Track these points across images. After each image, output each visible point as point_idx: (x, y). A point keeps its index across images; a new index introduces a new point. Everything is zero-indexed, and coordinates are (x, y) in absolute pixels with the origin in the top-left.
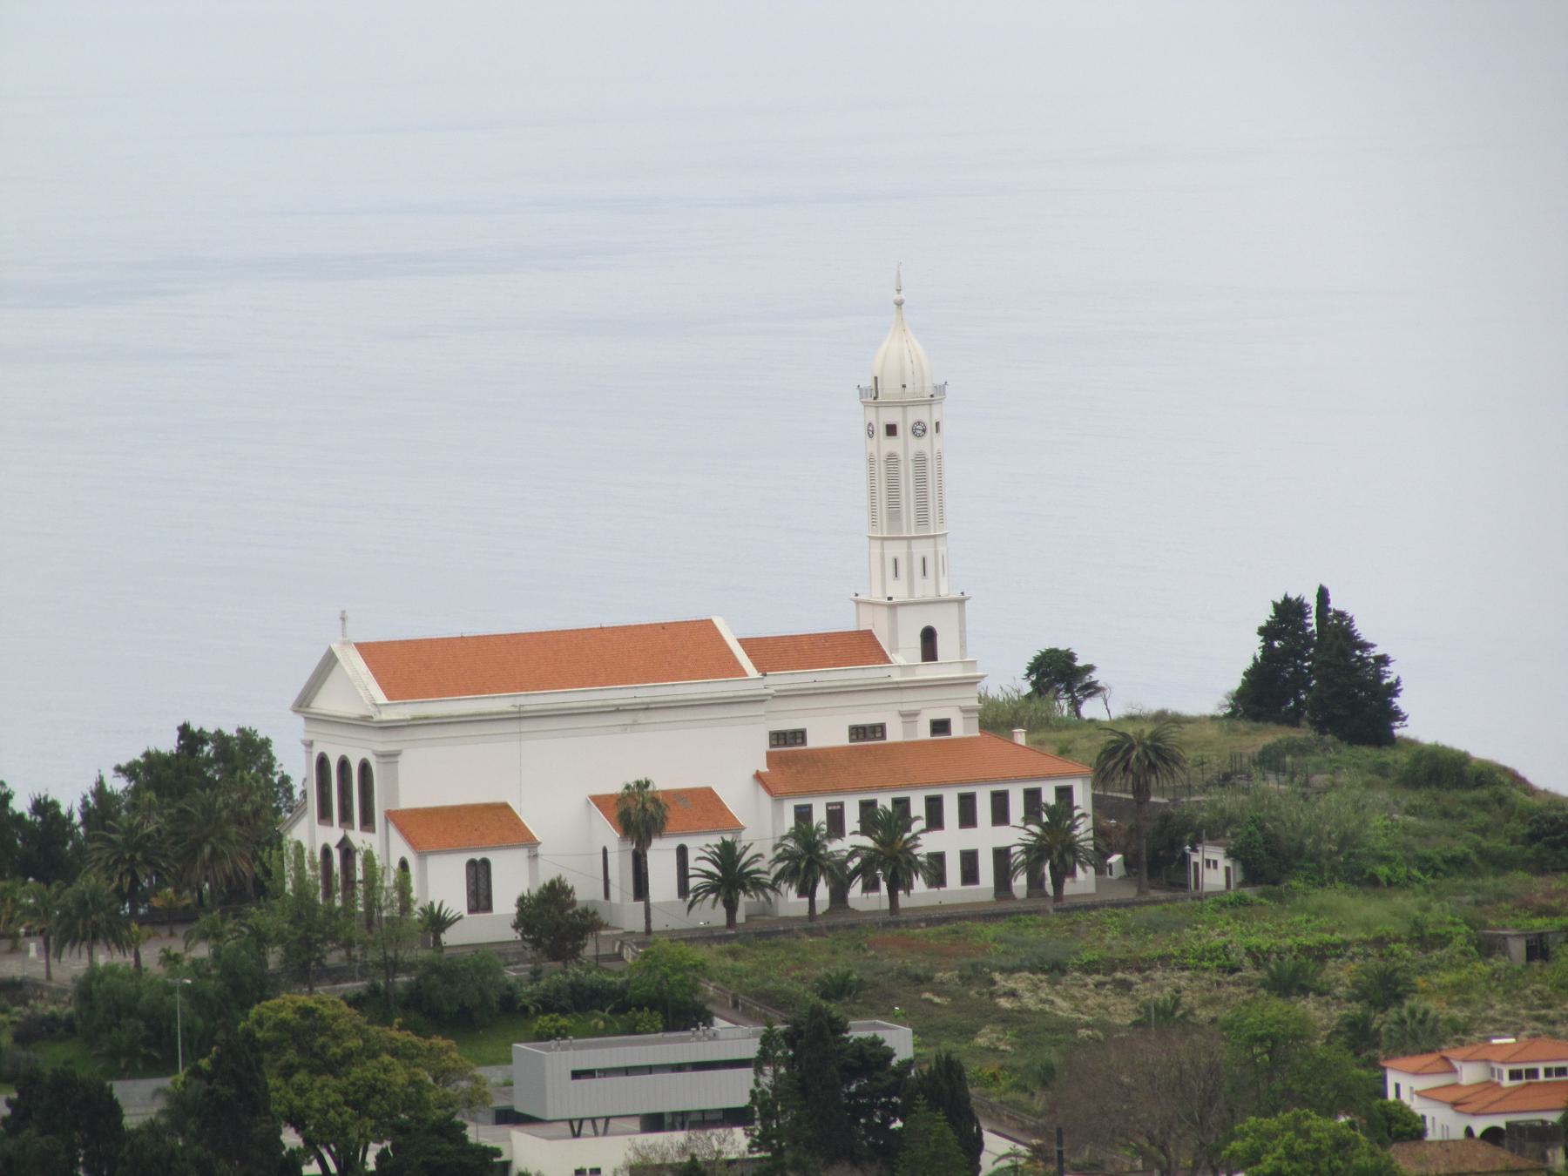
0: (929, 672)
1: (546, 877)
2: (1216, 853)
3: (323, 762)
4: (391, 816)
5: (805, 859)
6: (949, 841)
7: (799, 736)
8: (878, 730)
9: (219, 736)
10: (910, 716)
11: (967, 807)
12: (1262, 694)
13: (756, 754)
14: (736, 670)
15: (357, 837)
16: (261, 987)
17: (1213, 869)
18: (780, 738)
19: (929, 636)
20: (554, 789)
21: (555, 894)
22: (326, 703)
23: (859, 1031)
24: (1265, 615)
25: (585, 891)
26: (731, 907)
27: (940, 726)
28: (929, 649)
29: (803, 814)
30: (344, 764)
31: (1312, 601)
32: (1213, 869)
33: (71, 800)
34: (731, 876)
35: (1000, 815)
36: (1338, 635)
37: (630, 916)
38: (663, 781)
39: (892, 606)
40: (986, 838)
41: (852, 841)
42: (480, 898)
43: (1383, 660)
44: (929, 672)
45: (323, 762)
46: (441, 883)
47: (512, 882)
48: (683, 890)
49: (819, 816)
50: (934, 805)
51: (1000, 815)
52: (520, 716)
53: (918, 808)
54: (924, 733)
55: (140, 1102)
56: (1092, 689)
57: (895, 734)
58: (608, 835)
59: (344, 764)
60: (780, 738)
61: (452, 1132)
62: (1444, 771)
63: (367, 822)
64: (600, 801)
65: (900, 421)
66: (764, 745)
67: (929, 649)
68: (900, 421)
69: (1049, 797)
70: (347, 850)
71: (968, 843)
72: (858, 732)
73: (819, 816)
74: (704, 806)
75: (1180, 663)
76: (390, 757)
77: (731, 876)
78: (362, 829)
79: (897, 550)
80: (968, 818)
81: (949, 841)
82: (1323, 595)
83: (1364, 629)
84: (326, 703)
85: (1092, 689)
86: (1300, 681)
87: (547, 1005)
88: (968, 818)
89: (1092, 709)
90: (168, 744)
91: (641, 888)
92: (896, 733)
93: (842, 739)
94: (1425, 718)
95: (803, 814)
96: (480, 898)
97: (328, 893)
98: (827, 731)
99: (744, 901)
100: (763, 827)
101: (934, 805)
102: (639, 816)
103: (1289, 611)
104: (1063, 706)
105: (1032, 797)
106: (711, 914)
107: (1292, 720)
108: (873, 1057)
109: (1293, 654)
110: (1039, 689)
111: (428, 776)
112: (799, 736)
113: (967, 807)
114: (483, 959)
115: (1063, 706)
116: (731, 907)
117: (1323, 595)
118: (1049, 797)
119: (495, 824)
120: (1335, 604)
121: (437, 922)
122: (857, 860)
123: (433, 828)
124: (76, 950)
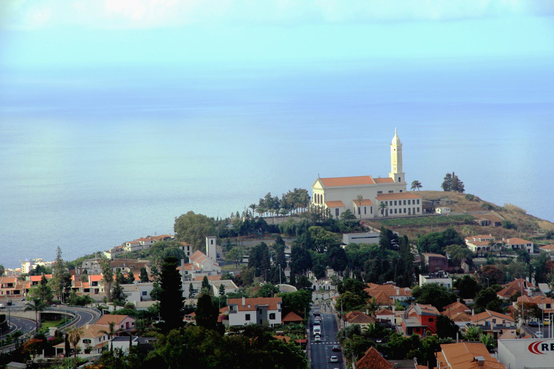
3: (315, 195)
8: (392, 191)
12: (445, 186)
13: (376, 194)
21: (348, 211)
24: (445, 176)
30: (318, 195)
31: (452, 174)
33: (280, 198)
42: (337, 214)
43: (462, 183)
44: (400, 183)
49: (384, 202)
50: (391, 202)
52: (333, 189)
56: (421, 186)
59: (318, 195)
62: (471, 198)
66: (376, 193)
72: (390, 192)
75: (433, 184)
82: (454, 173)
83: (459, 178)
91: (359, 213)
93: (388, 193)
97: (359, 213)
101: (391, 202)
103: (449, 175)
117: (454, 173)
120: (455, 175)
124: (219, 219)
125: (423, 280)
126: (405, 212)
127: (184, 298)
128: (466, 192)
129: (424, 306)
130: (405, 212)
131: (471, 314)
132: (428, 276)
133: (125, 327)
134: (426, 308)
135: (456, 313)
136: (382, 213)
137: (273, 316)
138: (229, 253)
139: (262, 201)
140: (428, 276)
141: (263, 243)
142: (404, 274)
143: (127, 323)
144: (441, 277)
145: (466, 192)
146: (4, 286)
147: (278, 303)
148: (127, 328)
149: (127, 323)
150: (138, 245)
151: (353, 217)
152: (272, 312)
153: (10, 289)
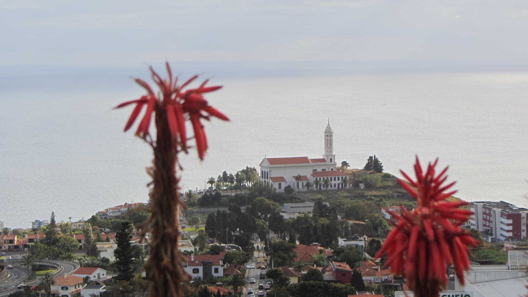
0: (331, 163)
1: (287, 185)
2: (362, 184)
3: (262, 172)
4: (270, 178)
5: (317, 182)
6: (333, 182)
7: (316, 170)
8: (325, 170)
9: (251, 168)
10: (329, 168)
11: (335, 178)
12: (367, 167)
13: (311, 172)
14: (309, 162)
15: (266, 180)
16: (256, 196)
17: (362, 186)
18: (314, 170)
19: (331, 159)
20: (289, 175)
21: (289, 187)
22: (263, 165)
23: (324, 203)
24: (368, 158)
25: (292, 187)
26: (308, 188)
27: (332, 169)
28: (331, 161)
29: (316, 179)
32: (362, 186)
34: (308, 185)
35: (339, 180)
36: (376, 161)
37: (296, 190)
38: (302, 175)
39: (327, 156)
40: (337, 182)
41: (322, 183)
42: (280, 187)
44: (331, 163)
45: (262, 172)
46: (276, 185)
47: (284, 185)
48: (303, 187)
49: (318, 179)
50: (331, 178)
51: (339, 180)
52: (285, 167)
53: (329, 178)
54: (330, 170)
55: (243, 209)
56: (349, 166)
57: (327, 170)
58: (294, 181)
60: (314, 170)
61: (278, 213)
63: (267, 178)
64: (294, 177)
65: (329, 135)
67: (331, 161)
68: (329, 135)
69: (344, 177)
70: (265, 181)
71: (335, 183)
72: (323, 170)
73: (318, 179)
74: (305, 178)
75: (358, 164)
76: (270, 171)
77: (308, 185)
78: (137, 134)
79: (328, 149)
80: (335, 180)
81: (333, 182)
83: (379, 160)
84: (263, 165)
85: (349, 166)
86: (372, 165)
87: (380, 187)
88: (335, 180)
89: (348, 168)
90: (245, 169)
91: (298, 187)
92: (327, 170)
93: (321, 170)
94: (385, 171)
95: (316, 179)
96: (280, 187)
98: (319, 170)
99: (310, 188)
100: (312, 180)
101: (331, 178)
102: (298, 178)
104: (345, 167)
105: (342, 178)
106: (305, 189)
107: (371, 170)
108: (325, 206)
109: (371, 162)
110: (343, 166)
111: (275, 174)
112: (316, 170)
113: (335, 178)
114: (280, 195)
115: (345, 167)
116: (308, 188)
118: (344, 177)
119: (282, 179)
121: (275, 189)
122: (307, 209)
123: (275, 179)
125: (342, 242)
126: (335, 186)
127: (219, 293)
128: (385, 171)
129: (338, 264)
130: (335, 186)
131: (377, 270)
132: (345, 239)
133: (97, 277)
134: (340, 266)
135: (236, 195)
136: (317, 187)
137: (216, 271)
138: (248, 253)
139: (219, 177)
140: (345, 239)
141: (218, 210)
142: (327, 236)
143: (99, 274)
144: (356, 240)
145: (385, 171)
146: (6, 242)
147: (221, 260)
148: (99, 278)
149: (99, 274)
150: (118, 210)
151: (292, 190)
152: (216, 267)
153: (11, 245)
